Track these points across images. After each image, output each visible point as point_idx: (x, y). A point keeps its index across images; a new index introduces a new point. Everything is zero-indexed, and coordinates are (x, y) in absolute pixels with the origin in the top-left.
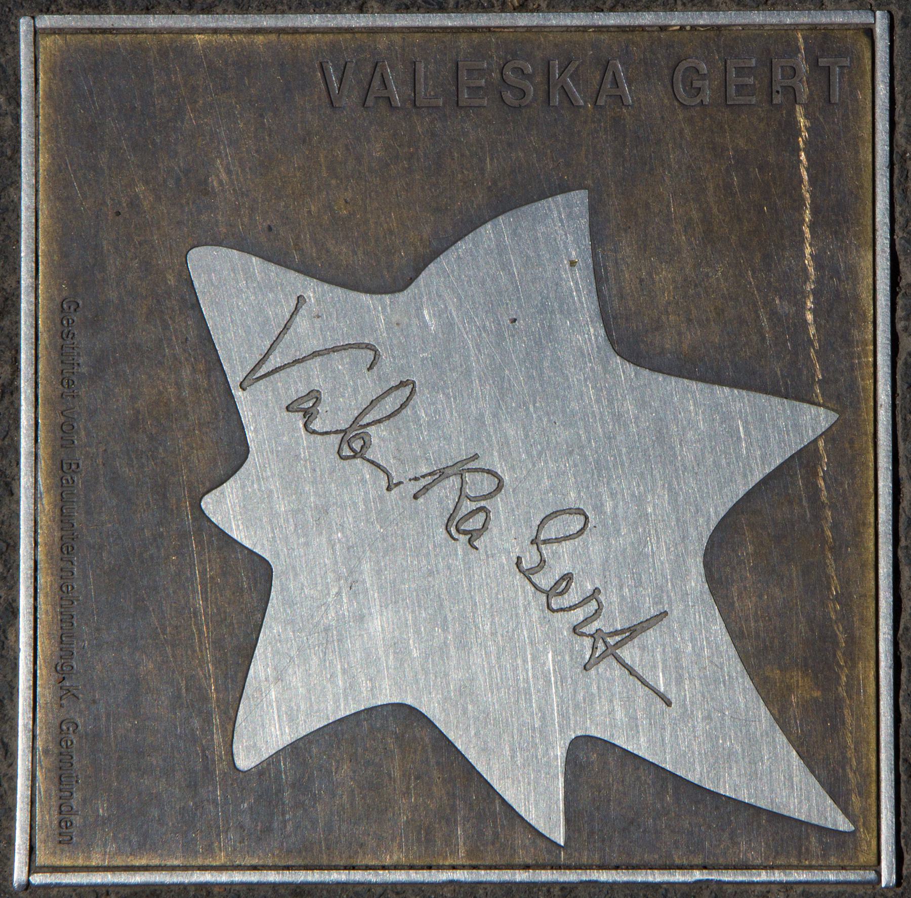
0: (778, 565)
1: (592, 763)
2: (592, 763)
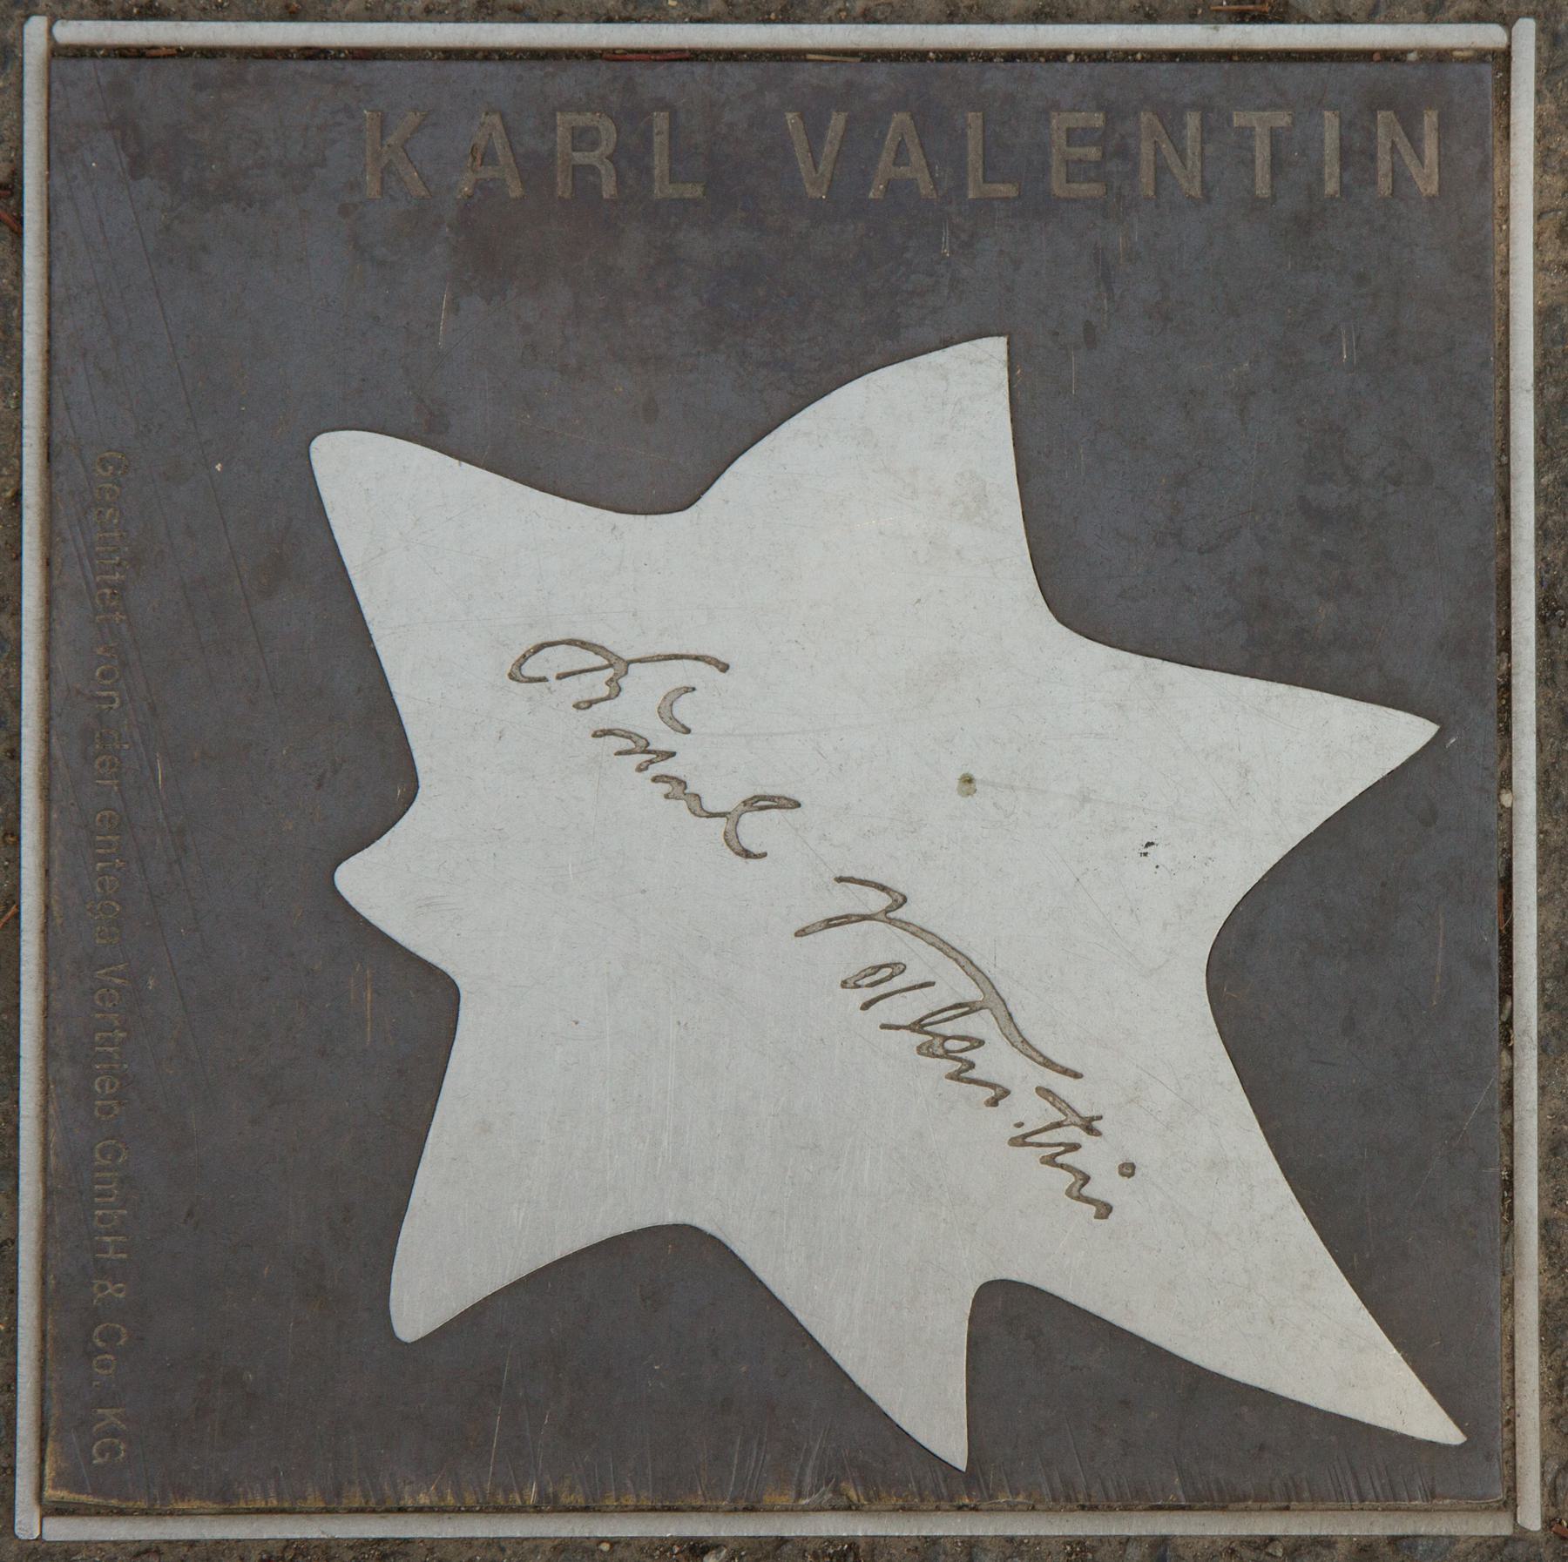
1: (1017, 1327)
2: (1017, 1327)
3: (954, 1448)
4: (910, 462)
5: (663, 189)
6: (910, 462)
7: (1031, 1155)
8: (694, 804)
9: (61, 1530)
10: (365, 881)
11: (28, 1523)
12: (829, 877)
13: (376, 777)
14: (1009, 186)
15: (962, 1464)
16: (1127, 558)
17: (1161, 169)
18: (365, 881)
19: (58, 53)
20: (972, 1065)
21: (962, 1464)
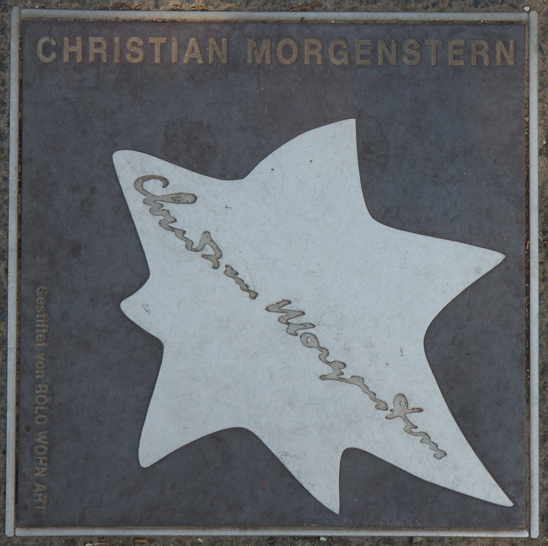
0: (467, 351)
1: (357, 465)
2: (357, 465)
3: (334, 506)
4: (323, 159)
5: (359, 62)
6: (323, 159)
7: (275, 316)
8: (373, 396)
9: (21, 532)
10: (131, 307)
11: (10, 530)
12: (316, 327)
13: (137, 274)
14: (212, 61)
15: (337, 511)
16: (399, 193)
17: (502, 56)
18: (131, 307)
19: (24, 24)
20: (343, 374)
21: (337, 511)
